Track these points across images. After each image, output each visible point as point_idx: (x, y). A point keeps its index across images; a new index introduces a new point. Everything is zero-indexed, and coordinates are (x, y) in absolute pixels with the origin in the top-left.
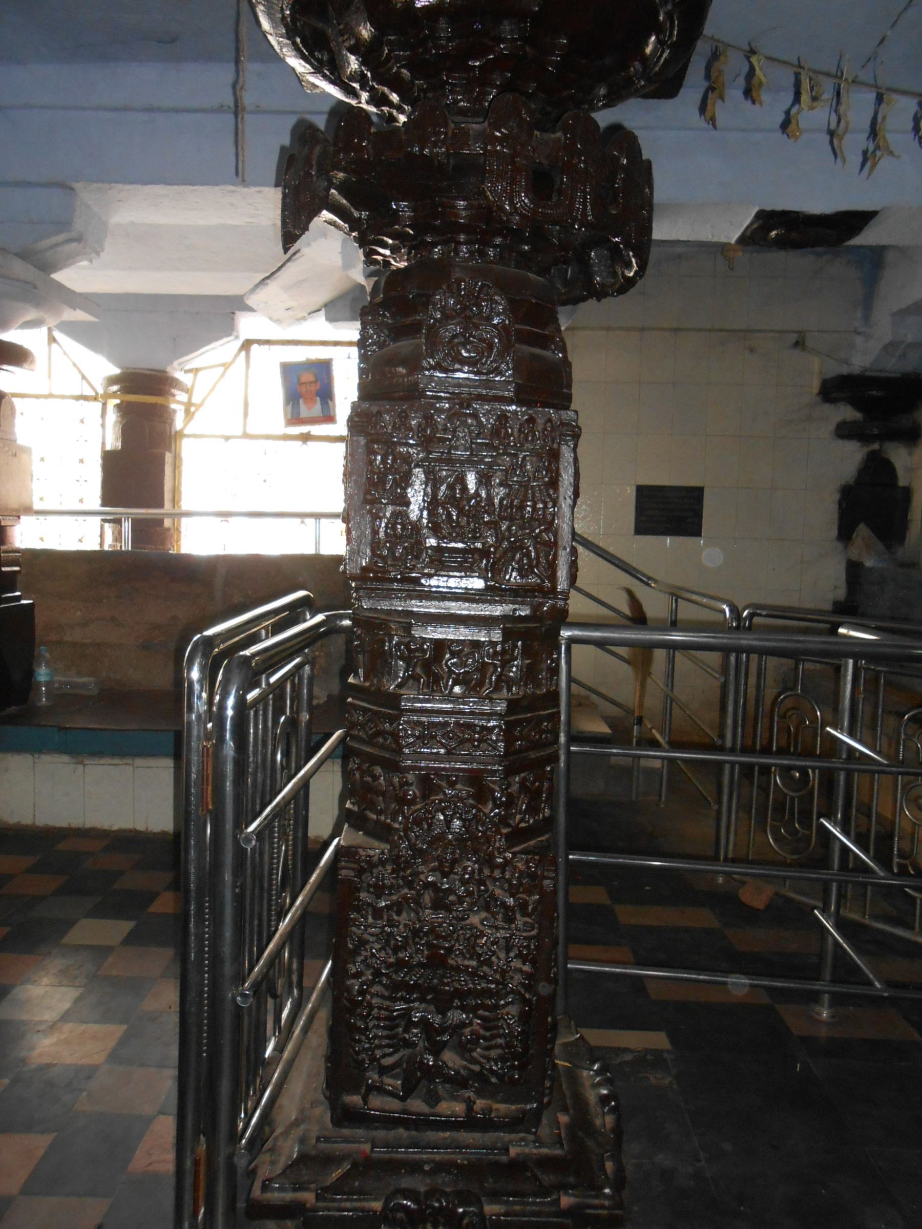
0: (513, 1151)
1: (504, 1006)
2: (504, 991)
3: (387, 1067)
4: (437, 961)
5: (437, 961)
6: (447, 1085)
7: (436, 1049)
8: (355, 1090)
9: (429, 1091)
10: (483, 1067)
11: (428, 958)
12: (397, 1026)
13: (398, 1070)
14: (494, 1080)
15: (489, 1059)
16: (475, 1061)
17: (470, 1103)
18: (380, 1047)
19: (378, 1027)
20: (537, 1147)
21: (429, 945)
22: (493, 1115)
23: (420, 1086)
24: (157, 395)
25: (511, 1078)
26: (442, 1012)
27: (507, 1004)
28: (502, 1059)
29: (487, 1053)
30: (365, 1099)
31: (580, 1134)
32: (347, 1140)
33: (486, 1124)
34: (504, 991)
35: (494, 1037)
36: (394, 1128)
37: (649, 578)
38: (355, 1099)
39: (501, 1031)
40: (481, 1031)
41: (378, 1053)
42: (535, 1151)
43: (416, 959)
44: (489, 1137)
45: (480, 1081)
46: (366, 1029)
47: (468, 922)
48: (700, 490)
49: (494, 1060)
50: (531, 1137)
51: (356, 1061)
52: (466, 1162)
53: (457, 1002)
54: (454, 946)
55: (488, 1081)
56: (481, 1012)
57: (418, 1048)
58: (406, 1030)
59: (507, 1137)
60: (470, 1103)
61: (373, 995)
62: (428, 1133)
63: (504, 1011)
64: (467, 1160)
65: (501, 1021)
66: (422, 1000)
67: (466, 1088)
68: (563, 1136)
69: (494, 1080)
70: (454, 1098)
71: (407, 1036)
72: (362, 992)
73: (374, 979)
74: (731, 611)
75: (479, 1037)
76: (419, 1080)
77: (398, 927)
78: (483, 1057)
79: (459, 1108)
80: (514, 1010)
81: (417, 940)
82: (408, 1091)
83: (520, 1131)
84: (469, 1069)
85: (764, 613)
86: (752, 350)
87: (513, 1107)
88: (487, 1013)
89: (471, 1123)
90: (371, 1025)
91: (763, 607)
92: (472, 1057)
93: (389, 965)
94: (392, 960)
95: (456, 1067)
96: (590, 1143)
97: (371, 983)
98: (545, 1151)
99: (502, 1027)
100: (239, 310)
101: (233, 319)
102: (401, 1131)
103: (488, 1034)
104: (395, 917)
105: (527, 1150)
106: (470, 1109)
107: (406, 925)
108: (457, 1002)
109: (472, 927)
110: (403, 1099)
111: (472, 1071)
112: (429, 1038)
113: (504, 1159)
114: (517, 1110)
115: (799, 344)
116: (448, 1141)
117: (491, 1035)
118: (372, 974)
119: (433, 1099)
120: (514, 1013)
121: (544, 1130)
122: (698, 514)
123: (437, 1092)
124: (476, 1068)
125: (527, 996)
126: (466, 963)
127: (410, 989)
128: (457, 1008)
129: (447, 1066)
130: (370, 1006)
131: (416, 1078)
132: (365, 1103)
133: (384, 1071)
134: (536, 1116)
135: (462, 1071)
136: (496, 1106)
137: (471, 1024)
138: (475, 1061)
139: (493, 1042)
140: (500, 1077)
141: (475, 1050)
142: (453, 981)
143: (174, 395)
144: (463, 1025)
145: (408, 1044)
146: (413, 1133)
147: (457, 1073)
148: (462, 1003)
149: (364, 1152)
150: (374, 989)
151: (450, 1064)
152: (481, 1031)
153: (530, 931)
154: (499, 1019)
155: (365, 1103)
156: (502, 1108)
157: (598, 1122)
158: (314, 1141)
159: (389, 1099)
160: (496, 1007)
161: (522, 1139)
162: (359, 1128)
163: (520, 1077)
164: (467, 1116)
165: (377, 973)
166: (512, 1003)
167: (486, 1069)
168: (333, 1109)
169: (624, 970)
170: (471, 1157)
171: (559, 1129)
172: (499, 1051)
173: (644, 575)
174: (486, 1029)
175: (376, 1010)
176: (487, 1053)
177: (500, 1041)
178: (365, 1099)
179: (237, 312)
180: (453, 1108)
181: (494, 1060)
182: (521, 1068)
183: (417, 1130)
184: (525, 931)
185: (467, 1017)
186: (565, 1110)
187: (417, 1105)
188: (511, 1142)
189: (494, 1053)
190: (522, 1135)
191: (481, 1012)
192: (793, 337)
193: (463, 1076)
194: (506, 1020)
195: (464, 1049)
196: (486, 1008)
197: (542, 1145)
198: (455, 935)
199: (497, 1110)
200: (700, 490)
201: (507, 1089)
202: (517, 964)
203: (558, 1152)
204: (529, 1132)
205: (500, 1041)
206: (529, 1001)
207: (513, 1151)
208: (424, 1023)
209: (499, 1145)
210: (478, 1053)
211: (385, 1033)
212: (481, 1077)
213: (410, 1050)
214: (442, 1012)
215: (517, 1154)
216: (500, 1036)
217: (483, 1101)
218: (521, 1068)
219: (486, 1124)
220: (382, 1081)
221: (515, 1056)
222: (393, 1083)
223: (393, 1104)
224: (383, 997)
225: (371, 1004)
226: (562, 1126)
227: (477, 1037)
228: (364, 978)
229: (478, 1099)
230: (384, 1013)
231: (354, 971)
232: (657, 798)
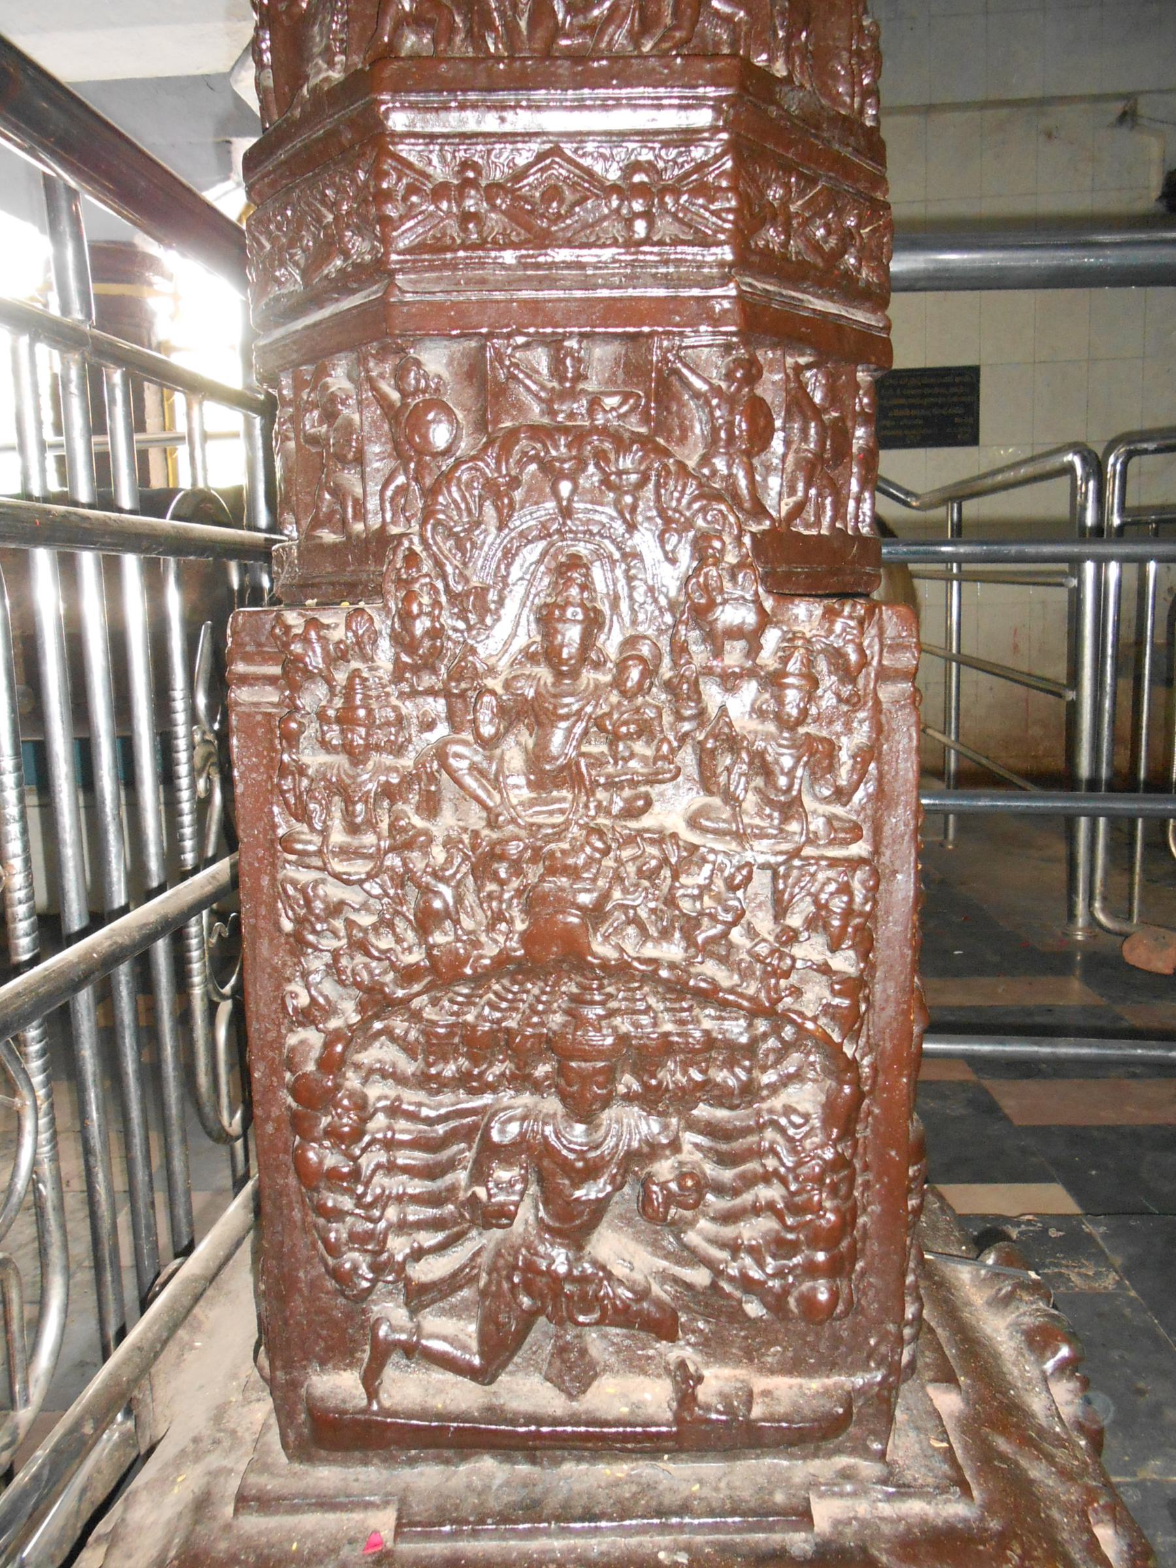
0: (826, 1513)
1: (774, 1089)
2: (772, 1042)
3: (424, 1288)
4: (553, 951)
5: (553, 951)
6: (613, 1330)
7: (574, 1224)
8: (338, 1352)
9: (562, 1350)
10: (718, 1273)
11: (526, 939)
12: (451, 1165)
13: (465, 1293)
14: (754, 1309)
15: (734, 1248)
16: (695, 1258)
17: (686, 1382)
18: (403, 1227)
19: (391, 1168)
20: (889, 1497)
21: (532, 901)
22: (757, 1411)
23: (532, 1336)
24: (122, 282)
25: (808, 1302)
26: (583, 1109)
27: (787, 1080)
28: (781, 1247)
29: (728, 1232)
30: (371, 1381)
31: (1002, 1444)
32: (326, 1503)
33: (737, 1435)
34: (772, 1042)
35: (749, 1181)
36: (464, 1458)
37: (908, 493)
38: (339, 1385)
39: (771, 1163)
40: (710, 1169)
41: (399, 1246)
42: (886, 1509)
43: (491, 950)
44: (747, 1475)
45: (715, 1312)
46: (355, 1175)
47: (646, 821)
48: (975, 371)
49: (753, 1251)
50: (868, 1469)
51: (335, 1273)
52: (683, 1558)
53: (628, 1082)
54: (605, 896)
55: (737, 1315)
56: (702, 1111)
57: (518, 1226)
58: (479, 1175)
59: (801, 1469)
60: (686, 1382)
61: (369, 1074)
62: (568, 1467)
63: (777, 1103)
64: (688, 1548)
65: (769, 1134)
66: (521, 1080)
67: (672, 1338)
68: (959, 1453)
69: (754, 1309)
70: (636, 1365)
71: (481, 1192)
72: (330, 1063)
73: (365, 1023)
74: (1084, 460)
75: (703, 1185)
76: (528, 1320)
77: (425, 849)
78: (713, 1241)
79: (652, 1397)
80: (806, 1098)
81: (491, 887)
82: (498, 1350)
83: (838, 1451)
84: (676, 1280)
85: (1151, 446)
86: (1049, 136)
87: (815, 1384)
88: (722, 1114)
89: (694, 1432)
90: (367, 1163)
91: (1145, 436)
92: (685, 1247)
93: (408, 975)
94: (416, 957)
95: (638, 1276)
96: (1037, 1471)
97: (360, 1035)
98: (915, 1507)
99: (773, 1151)
100: (237, 136)
101: (229, 152)
102: (487, 1464)
103: (727, 1175)
104: (418, 822)
105: (862, 1508)
106: (686, 1398)
107: (450, 843)
108: (628, 1082)
109: (662, 838)
110: (483, 1375)
111: (689, 1286)
112: (550, 1195)
113: (799, 1542)
114: (826, 1393)
115: (1128, 118)
116: (627, 1492)
117: (742, 1177)
118: (361, 1007)
119: (574, 1371)
120: (806, 1106)
121: (905, 1445)
122: (972, 410)
123: (583, 1352)
124: (700, 1277)
125: (849, 1050)
126: (650, 951)
127: (479, 1045)
128: (629, 1098)
129: (609, 1275)
130: (361, 1105)
131: (523, 1309)
132: (372, 1393)
133: (419, 1297)
134: (882, 1404)
135: (656, 1289)
136: (761, 1383)
137: (675, 1146)
138: (695, 1258)
139: (747, 1198)
140: (776, 1303)
141: (692, 1224)
142: (612, 1014)
143: (150, 284)
144: (652, 1151)
145: (494, 1216)
146: (524, 1468)
147: (643, 1294)
148: (645, 1085)
149: (373, 1542)
150: (370, 1056)
151: (619, 1270)
152: (710, 1169)
153: (845, 843)
154: (761, 1128)
155: (372, 1393)
156: (783, 1392)
157: (1037, 1404)
158: (230, 1510)
159: (440, 1376)
160: (749, 1092)
161: (846, 1475)
162: (365, 1463)
163: (835, 1295)
164: (678, 1420)
165: (376, 1002)
166: (797, 1077)
167: (731, 1279)
168: (284, 1412)
169: (1000, 1048)
170: (699, 1539)
171: (944, 1436)
172: (766, 1223)
173: (899, 489)
174: (724, 1160)
175: (381, 1120)
176: (728, 1232)
177: (771, 1193)
178: (371, 1381)
179: (234, 140)
180: (633, 1392)
181: (753, 1251)
182: (837, 1268)
183: (533, 1461)
184: (831, 843)
185: (665, 1127)
186: (947, 1377)
187: (527, 1391)
188: (812, 1484)
189: (752, 1231)
190: (842, 1461)
191: (702, 1111)
192: (1118, 107)
193: (658, 1303)
194: (782, 1131)
195: (656, 1216)
196: (722, 1097)
197: (905, 1490)
198: (608, 862)
199: (766, 1393)
200: (975, 371)
201: (805, 1332)
202: (811, 949)
203: (954, 1509)
204: (866, 1453)
205: (771, 1193)
206: (853, 1064)
207: (826, 1513)
208: (540, 1159)
209: (779, 1498)
210: (700, 1233)
211: (416, 1187)
212: (713, 1302)
213: (498, 1233)
214: (583, 1109)
215: (836, 1523)
216: (766, 1178)
217: (727, 1371)
218: (837, 1268)
219: (737, 1435)
220: (419, 1327)
221: (816, 1239)
222: (453, 1330)
223: (459, 1396)
224: (400, 1079)
225: (365, 1097)
226: (949, 1425)
227: (695, 1189)
228: (334, 1023)
229: (707, 1365)
230: (405, 1130)
231: (304, 1000)
232: (941, 838)
